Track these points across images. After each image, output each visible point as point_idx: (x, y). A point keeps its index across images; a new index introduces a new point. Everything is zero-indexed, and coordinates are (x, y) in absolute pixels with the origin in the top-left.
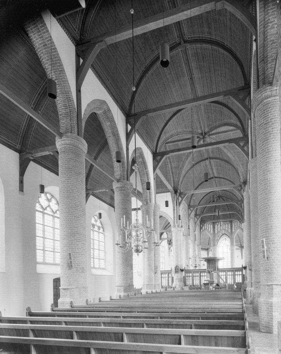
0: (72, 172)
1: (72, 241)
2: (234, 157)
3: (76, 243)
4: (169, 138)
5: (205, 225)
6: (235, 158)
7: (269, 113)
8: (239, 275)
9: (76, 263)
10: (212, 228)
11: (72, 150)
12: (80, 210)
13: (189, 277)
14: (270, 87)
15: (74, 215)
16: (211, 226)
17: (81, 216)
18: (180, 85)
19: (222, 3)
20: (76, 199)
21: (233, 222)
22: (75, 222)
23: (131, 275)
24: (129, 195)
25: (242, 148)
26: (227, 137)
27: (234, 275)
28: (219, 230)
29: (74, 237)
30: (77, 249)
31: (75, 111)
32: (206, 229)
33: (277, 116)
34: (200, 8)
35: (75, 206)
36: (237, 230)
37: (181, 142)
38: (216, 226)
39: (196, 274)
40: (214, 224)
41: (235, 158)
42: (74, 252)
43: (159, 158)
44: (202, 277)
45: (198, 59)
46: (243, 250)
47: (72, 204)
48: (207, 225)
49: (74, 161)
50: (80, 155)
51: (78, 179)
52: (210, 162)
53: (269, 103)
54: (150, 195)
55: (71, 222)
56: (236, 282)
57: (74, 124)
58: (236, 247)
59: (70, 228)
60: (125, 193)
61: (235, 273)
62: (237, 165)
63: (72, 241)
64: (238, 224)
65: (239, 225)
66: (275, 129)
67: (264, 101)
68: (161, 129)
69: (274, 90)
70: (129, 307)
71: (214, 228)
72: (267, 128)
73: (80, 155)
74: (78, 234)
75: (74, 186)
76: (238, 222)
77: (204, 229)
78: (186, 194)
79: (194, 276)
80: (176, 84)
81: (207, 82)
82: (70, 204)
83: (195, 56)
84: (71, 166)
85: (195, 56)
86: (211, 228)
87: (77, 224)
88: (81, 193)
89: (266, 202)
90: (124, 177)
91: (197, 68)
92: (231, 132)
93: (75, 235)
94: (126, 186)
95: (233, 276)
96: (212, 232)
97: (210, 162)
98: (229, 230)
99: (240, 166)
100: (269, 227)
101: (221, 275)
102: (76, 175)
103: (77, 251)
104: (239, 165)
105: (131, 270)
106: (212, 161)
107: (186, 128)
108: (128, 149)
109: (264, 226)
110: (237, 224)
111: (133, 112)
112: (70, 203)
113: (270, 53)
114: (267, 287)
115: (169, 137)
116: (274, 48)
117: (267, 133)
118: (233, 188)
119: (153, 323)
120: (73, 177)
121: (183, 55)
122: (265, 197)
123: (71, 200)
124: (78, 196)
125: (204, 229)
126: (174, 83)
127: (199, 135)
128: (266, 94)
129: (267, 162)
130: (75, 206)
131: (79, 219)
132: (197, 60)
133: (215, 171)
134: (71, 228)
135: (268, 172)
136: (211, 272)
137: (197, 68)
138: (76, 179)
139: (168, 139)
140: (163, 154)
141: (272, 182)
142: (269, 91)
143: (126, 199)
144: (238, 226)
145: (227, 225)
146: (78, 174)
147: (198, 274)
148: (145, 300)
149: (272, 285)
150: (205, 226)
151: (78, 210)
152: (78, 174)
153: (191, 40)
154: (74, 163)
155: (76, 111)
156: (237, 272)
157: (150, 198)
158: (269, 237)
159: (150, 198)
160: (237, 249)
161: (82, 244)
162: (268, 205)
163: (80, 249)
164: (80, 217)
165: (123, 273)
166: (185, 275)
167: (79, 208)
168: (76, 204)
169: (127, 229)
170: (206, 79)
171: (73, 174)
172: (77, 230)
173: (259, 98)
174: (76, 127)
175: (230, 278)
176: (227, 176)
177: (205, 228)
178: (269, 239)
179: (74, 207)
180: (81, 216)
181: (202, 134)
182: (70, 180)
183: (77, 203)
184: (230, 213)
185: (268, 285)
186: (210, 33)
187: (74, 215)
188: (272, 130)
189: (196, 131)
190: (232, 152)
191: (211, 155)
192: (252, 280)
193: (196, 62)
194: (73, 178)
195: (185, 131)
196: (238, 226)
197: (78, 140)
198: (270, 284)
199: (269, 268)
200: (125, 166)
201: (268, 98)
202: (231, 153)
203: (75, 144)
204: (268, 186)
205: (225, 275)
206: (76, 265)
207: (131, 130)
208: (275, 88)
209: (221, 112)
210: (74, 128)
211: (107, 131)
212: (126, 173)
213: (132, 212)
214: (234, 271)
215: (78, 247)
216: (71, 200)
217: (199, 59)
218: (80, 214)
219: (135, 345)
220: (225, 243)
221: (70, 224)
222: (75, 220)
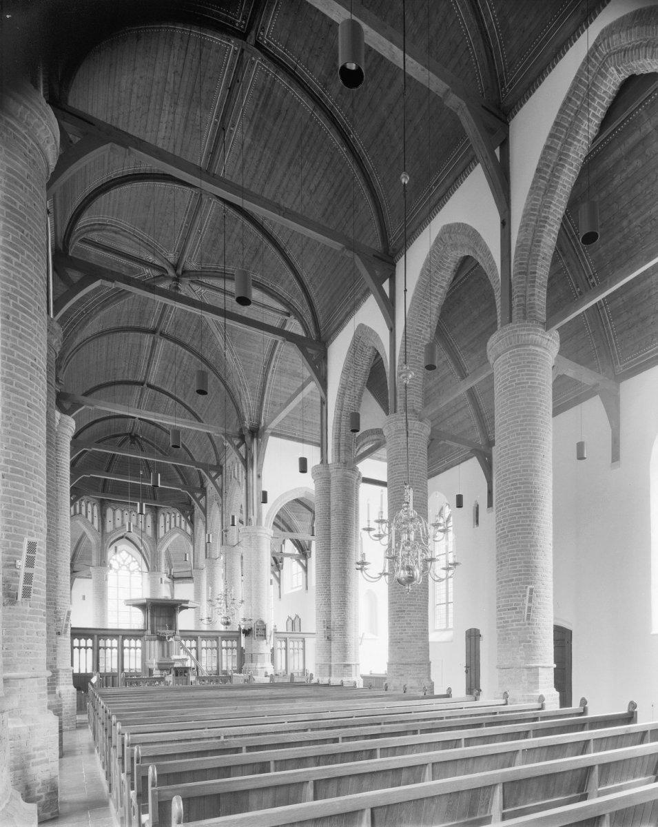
0: (26, 231)
4: (94, 230)
8: (86, 648)
13: (133, 650)
16: (95, 508)
18: (187, 118)
19: (459, 103)
21: (161, 511)
27: (96, 650)
28: (118, 523)
32: (80, 513)
34: (423, 70)
36: (173, 534)
39: (83, 643)
40: (103, 505)
45: (265, 105)
48: (83, 503)
52: (154, 344)
53: (537, 355)
56: (102, 671)
59: (14, 442)
61: (98, 644)
62: (240, 385)
64: (178, 519)
65: (180, 522)
67: (531, 347)
70: (335, 725)
71: (103, 516)
76: (178, 515)
79: (100, 648)
80: (179, 110)
81: (257, 167)
83: (261, 93)
85: (261, 93)
86: (93, 513)
89: (528, 523)
91: (251, 121)
96: (96, 525)
97: (154, 344)
98: (149, 531)
106: (162, 344)
107: (143, 229)
109: (523, 564)
114: (526, 672)
118: (223, 434)
121: (232, 64)
122: (526, 513)
126: (176, 104)
127: (168, 266)
128: (535, 337)
132: (261, 103)
133: (155, 369)
134: (17, 443)
136: (169, 638)
137: (251, 121)
139: (88, 231)
140: (93, 272)
144: (178, 524)
147: (115, 643)
149: (537, 667)
153: (271, 53)
156: (79, 639)
170: (260, 160)
173: (522, 335)
176: (185, 395)
181: (175, 267)
182: (18, 258)
184: (105, 479)
185: (529, 668)
186: (325, 85)
189: (162, 251)
191: (168, 328)
192: (331, 661)
193: (256, 107)
194: (28, 257)
196: (178, 524)
198: (533, 665)
199: (530, 637)
205: (196, 648)
209: (257, 251)
214: (96, 636)
216: (20, 336)
217: (269, 107)
220: (124, 561)
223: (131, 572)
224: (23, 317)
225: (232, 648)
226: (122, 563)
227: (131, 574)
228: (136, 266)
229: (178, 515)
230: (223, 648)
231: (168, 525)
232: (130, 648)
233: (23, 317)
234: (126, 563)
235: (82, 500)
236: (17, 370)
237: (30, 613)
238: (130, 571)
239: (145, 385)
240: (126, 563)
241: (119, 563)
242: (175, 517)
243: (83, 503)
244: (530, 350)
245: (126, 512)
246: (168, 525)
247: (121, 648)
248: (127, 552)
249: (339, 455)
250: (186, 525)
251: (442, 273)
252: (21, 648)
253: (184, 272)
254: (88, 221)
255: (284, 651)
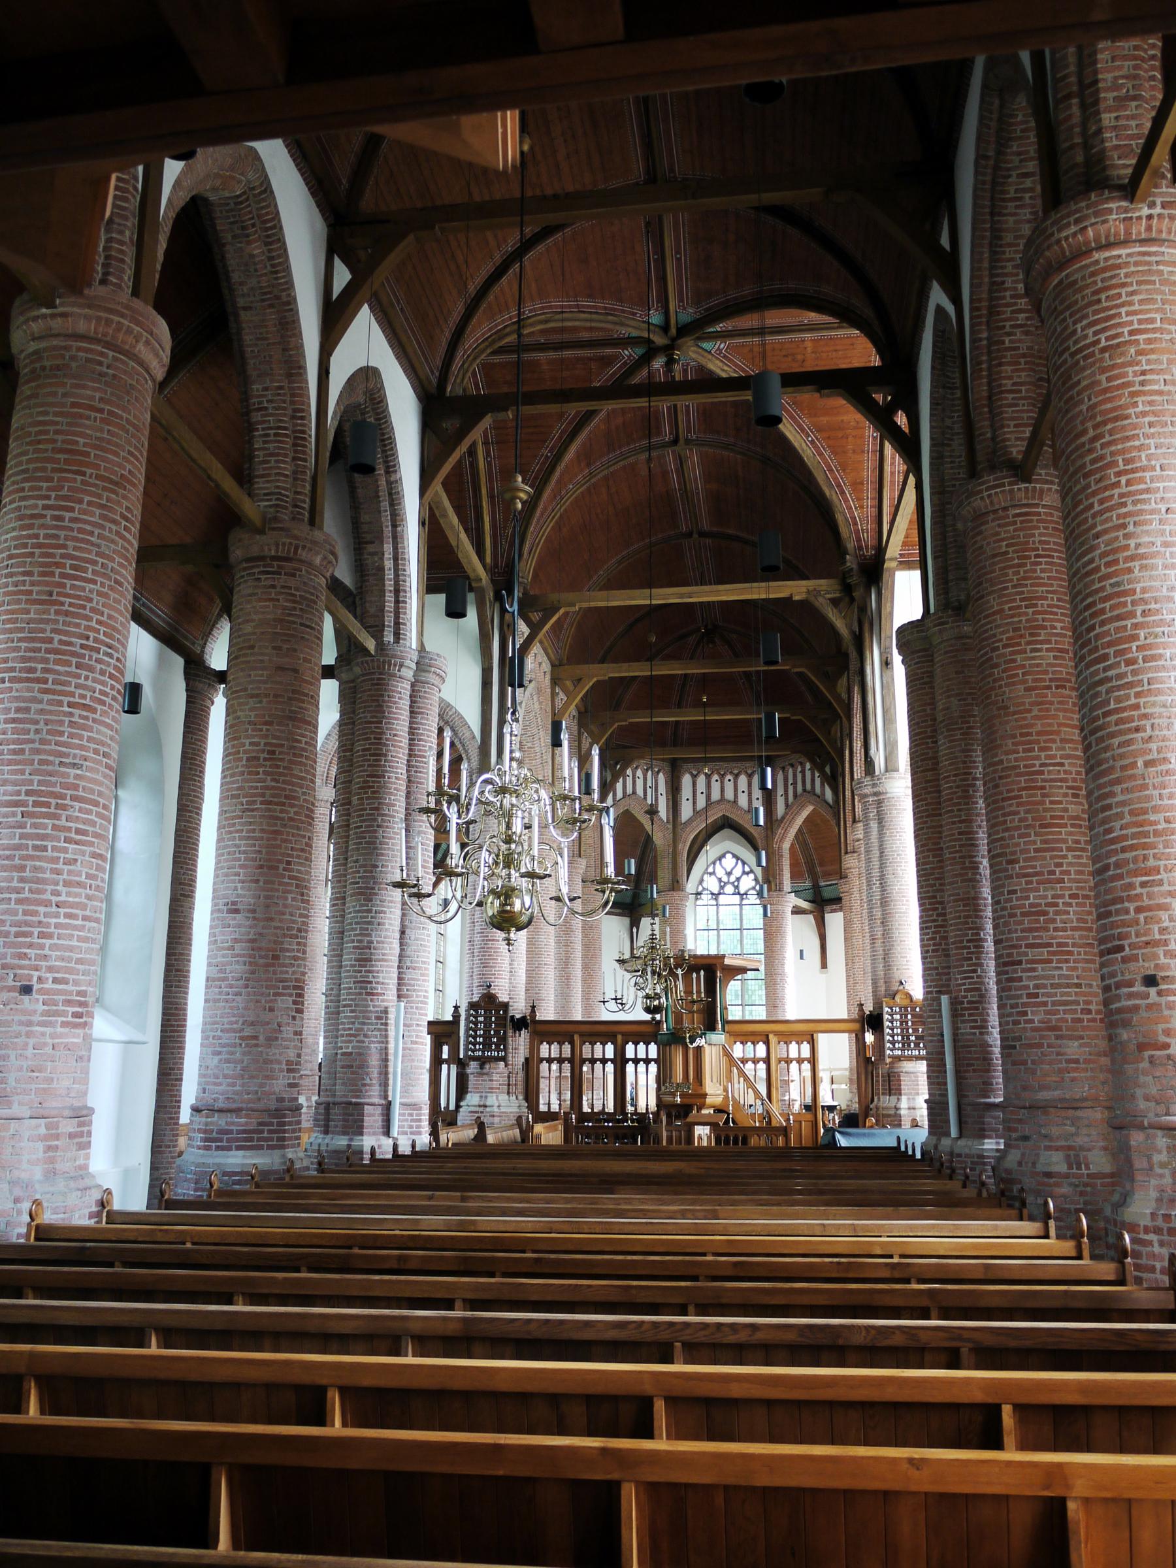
0: (89, 471)
1: (44, 837)
2: (816, 447)
3: (65, 850)
5: (629, 772)
6: (821, 454)
7: (1123, 305)
8: (647, 1061)
9: (50, 969)
10: (662, 788)
11: (100, 363)
12: (102, 673)
14: (1124, 204)
15: (72, 694)
16: (661, 778)
17: (103, 703)
20: (93, 610)
22: (71, 736)
23: (295, 1047)
24: (315, 603)
25: (882, 419)
26: (784, 353)
29: (58, 817)
30: (67, 884)
31: (136, 189)
32: (634, 792)
33: (1158, 324)
35: (82, 646)
36: (802, 807)
37: (553, 355)
38: (686, 780)
41: (821, 454)
42: (48, 903)
43: (450, 425)
44: (630, 1067)
46: (835, 921)
47: (66, 633)
48: (639, 773)
49: (102, 420)
50: (135, 394)
51: (110, 509)
53: (1119, 267)
54: (397, 602)
55: (49, 732)
57: (122, 243)
58: (793, 900)
60: (297, 589)
63: (44, 837)
64: (808, 774)
65: (813, 781)
66: (1155, 377)
67: (1096, 256)
68: (472, 289)
69: (1139, 218)
71: (674, 790)
72: (1113, 367)
73: (135, 394)
74: (74, 798)
75: (88, 542)
76: (808, 766)
77: (619, 795)
78: (559, 609)
82: (57, 637)
84: (85, 445)
87: (82, 748)
88: (116, 582)
90: (296, 506)
92: (808, 335)
93: (64, 807)
94: (303, 554)
95: (567, 1066)
99: (843, 493)
100: (1155, 823)
101: (744, 1061)
102: (105, 489)
103: (63, 898)
104: (839, 486)
105: (294, 1018)
108: (328, 373)
110: (799, 776)
111: (368, 203)
112: (53, 631)
113: (1109, 72)
115: (508, 330)
116: (1125, 58)
117: (1118, 387)
119: (731, 1339)
120: (87, 498)
123: (67, 613)
124: (106, 596)
125: (619, 795)
128: (1102, 229)
129: (1125, 515)
130: (82, 646)
131: (94, 720)
135: (1132, 558)
138: (102, 507)
141: (1157, 606)
142: (1115, 217)
143: (299, 621)
144: (808, 787)
145: (743, 780)
146: (116, 484)
148: (431, 1198)
150: (629, 780)
151: (91, 669)
152: (116, 484)
154: (102, 430)
155: (140, 186)
157: (397, 617)
158: (1159, 873)
159: (397, 617)
160: (797, 911)
161: (95, 855)
162: (1146, 716)
163: (79, 884)
164: (99, 707)
165: (248, 1032)
166: (534, 1049)
167: (98, 661)
168: (88, 638)
169: (458, 802)
171: (92, 481)
172: (77, 777)
173: (1067, 238)
174: (127, 260)
175: (555, 1074)
177: (629, 790)
178: (1160, 883)
179: (74, 654)
180: (103, 703)
183: (92, 634)
184: (677, 722)
187: (72, 694)
188: (1142, 378)
190: (806, 422)
195: (583, 306)
196: (808, 787)
197: (138, 323)
200: (304, 453)
201: (1109, 245)
202: (800, 426)
203: (121, 336)
204: (1136, 626)
205: (767, 1060)
206: (50, 976)
207: (350, 290)
208: (1146, 211)
210: (123, 261)
211: (241, 284)
212: (308, 487)
213: (323, 681)
214: (619, 1037)
215: (70, 872)
216: (67, 613)
218: (102, 693)
219: (900, 1459)
220: (729, 874)
221: (43, 741)
222: (72, 724)
223: (743, 896)
224: (73, 587)
225: (560, 1061)
226: (725, 879)
227: (742, 899)
228: (608, 351)
229: (808, 766)
230: (656, 1061)
231: (791, 789)
232: (550, 1061)
233: (73, 587)
234: (732, 879)
235: (637, 768)
236: (56, 662)
237: (42, 1015)
238: (739, 894)
239: (695, 536)
240: (732, 879)
241: (720, 880)
242: (803, 772)
243: (639, 773)
244: (1097, 262)
245: (729, 777)
246: (791, 789)
247: (620, 1062)
248: (734, 856)
249: (947, 593)
250: (822, 785)
251: (1015, 149)
252: (20, 1069)
253: (679, 330)
254: (490, 330)
255: (806, 1066)
